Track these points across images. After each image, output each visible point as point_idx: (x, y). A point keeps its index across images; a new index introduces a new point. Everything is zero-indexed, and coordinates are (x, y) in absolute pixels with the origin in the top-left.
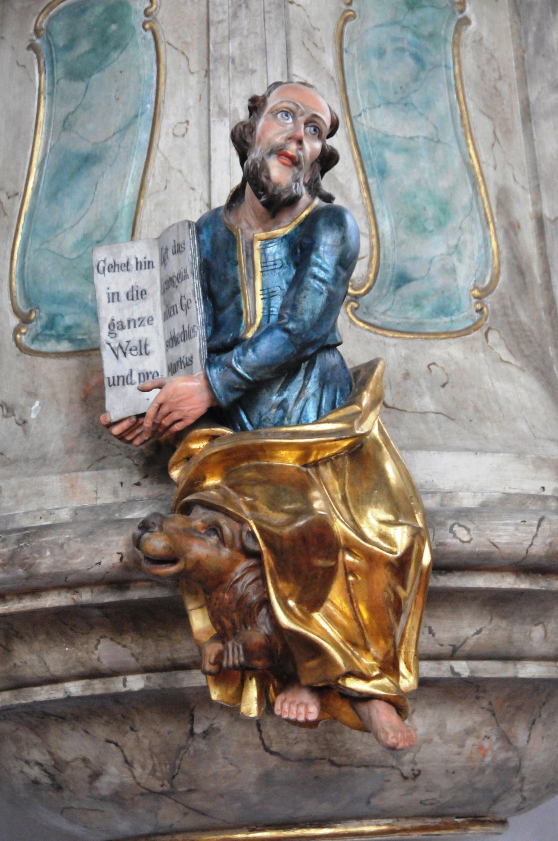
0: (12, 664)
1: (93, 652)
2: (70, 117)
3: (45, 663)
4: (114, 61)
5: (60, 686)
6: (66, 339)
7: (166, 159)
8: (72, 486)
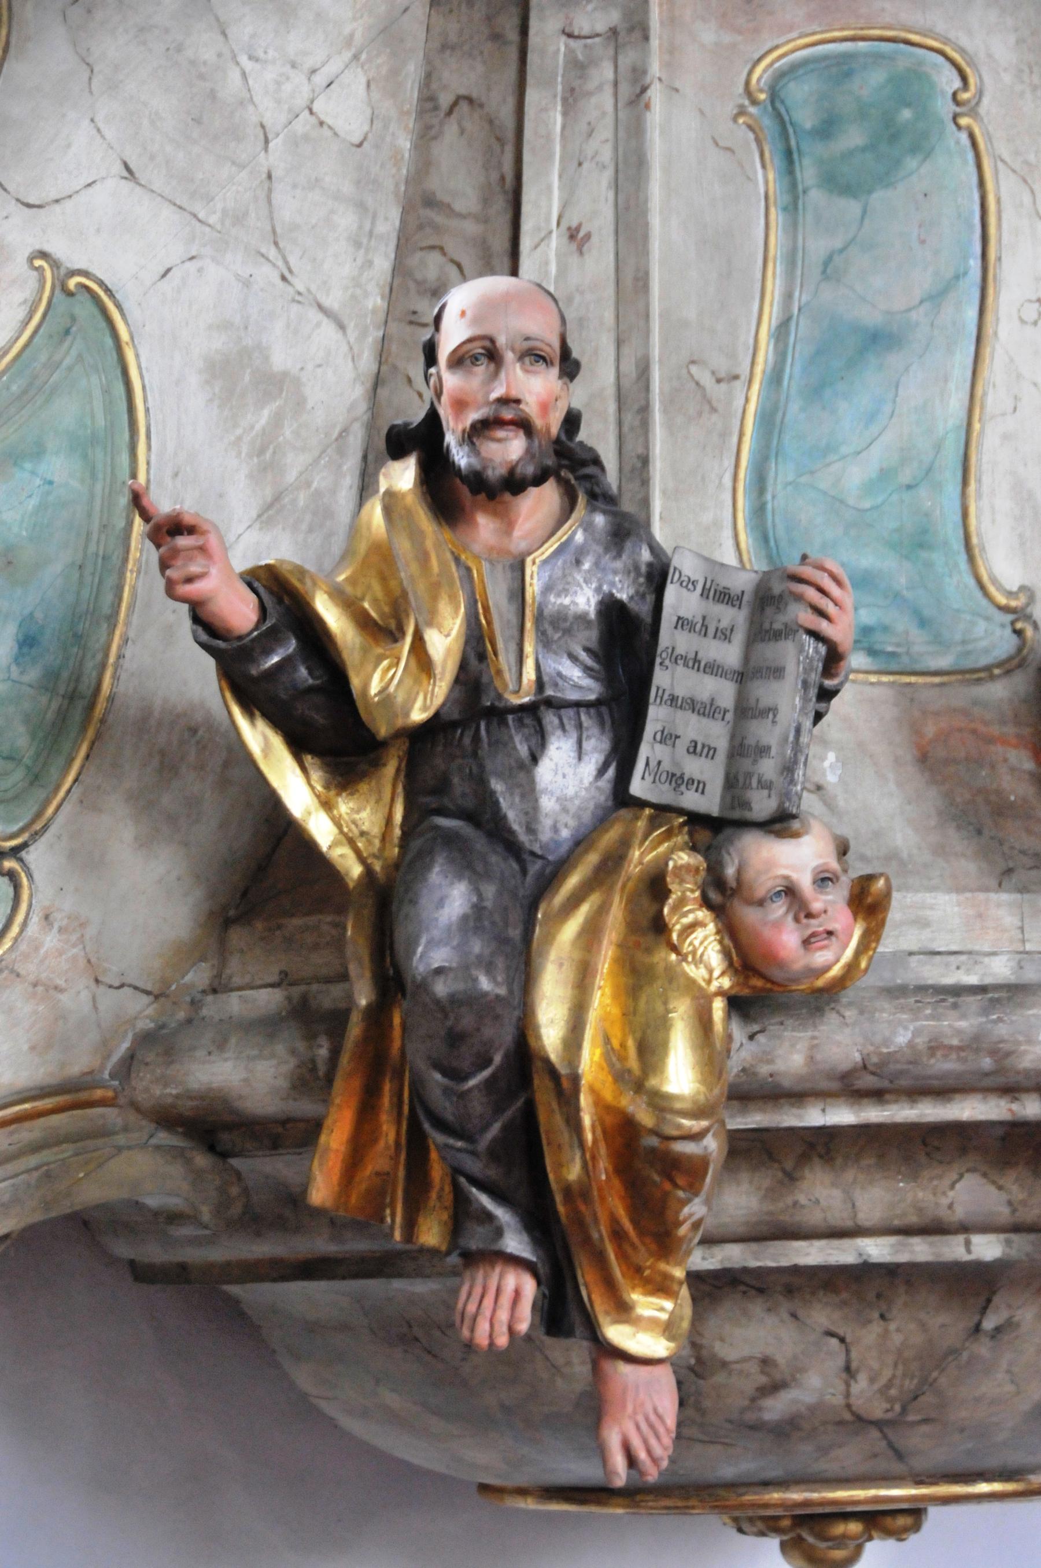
0: (789, 1200)
1: (944, 1193)
2: (837, 259)
3: (854, 1205)
4: (910, 174)
5: (846, 1243)
6: (863, 649)
7: (1012, 360)
8: (980, 916)
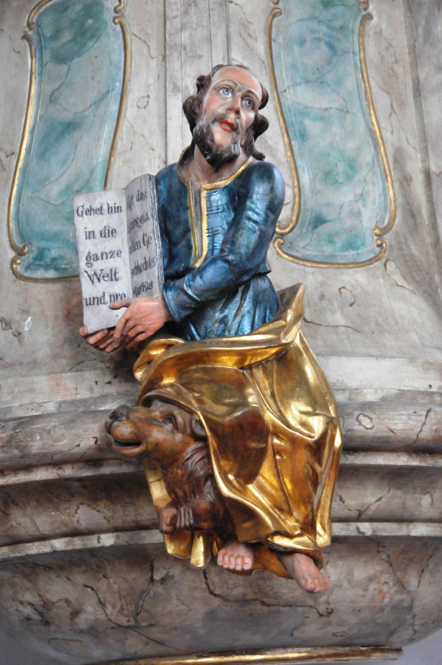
0: (9, 525)
1: (73, 516)
2: (56, 92)
4: (90, 48)
5: (47, 542)
6: (52, 268)
7: (131, 126)
8: (57, 384)
